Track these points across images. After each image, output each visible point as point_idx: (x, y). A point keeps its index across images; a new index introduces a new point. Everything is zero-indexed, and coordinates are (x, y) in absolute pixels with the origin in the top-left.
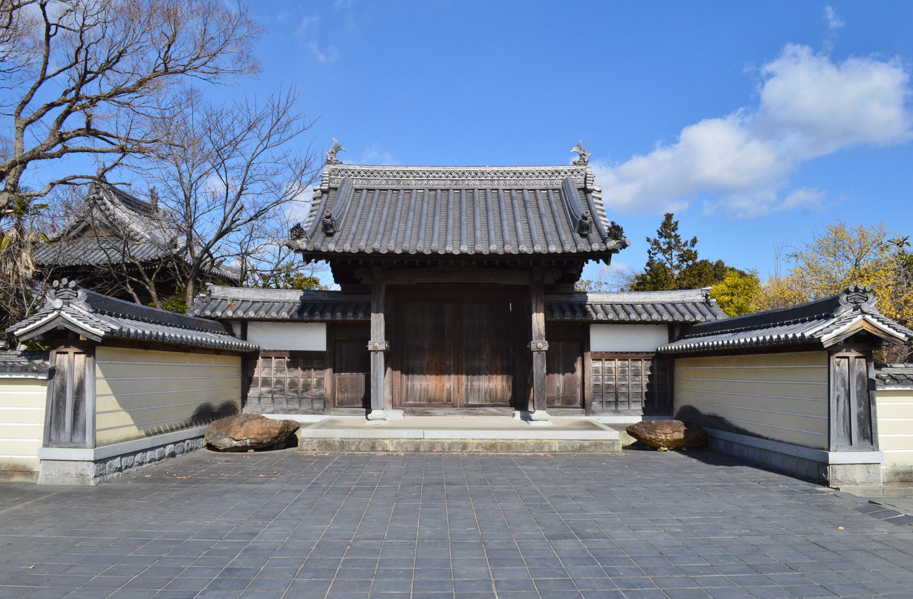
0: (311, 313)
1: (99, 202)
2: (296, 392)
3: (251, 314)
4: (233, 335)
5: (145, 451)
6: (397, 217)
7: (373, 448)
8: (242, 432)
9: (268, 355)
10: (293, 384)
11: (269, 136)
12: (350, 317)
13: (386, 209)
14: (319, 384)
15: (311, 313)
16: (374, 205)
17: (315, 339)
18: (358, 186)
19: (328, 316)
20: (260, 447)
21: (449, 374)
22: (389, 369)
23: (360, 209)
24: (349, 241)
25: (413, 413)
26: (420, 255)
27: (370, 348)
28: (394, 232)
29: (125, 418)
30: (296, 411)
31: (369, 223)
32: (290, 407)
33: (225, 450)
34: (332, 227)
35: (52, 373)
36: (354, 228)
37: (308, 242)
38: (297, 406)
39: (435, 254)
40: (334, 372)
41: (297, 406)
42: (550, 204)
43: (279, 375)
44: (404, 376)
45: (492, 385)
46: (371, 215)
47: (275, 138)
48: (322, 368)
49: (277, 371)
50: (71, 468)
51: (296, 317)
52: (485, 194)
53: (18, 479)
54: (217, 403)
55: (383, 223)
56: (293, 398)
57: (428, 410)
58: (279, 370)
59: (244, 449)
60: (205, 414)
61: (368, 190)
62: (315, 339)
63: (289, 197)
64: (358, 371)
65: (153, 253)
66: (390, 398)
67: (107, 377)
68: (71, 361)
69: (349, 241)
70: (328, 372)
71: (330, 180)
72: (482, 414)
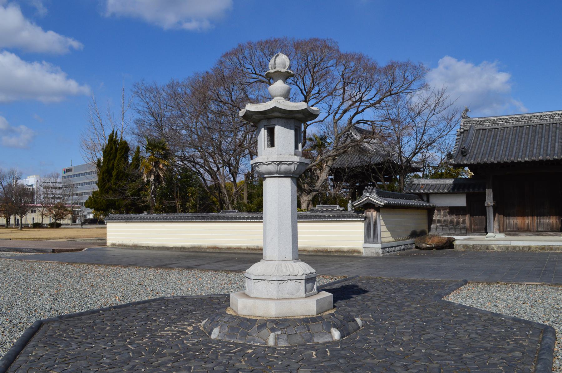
0: (458, 189)
1: (350, 136)
2: (453, 225)
3: (431, 191)
4: (423, 200)
5: (395, 247)
6: (496, 144)
7: (487, 248)
8: (430, 242)
9: (439, 209)
10: (452, 222)
11: (434, 109)
12: (476, 190)
13: (491, 140)
14: (464, 221)
15: (458, 189)
16: (485, 138)
17: (461, 201)
18: (478, 128)
19: (466, 191)
20: (438, 247)
21: (528, 216)
22: (497, 215)
23: (479, 141)
24: (473, 159)
25: (510, 235)
26: (506, 163)
27: (486, 205)
28: (494, 152)
29: (388, 234)
30: (454, 234)
31: (483, 148)
32: (450, 232)
33: (424, 249)
34: (465, 152)
35: (365, 218)
36: (475, 152)
37: (455, 160)
38: (454, 232)
39: (513, 162)
40: (471, 216)
41: (454, 232)
42: (389, 247)
43: (445, 218)
44: (505, 218)
45: (551, 221)
46: (484, 144)
47: (437, 110)
48: (465, 214)
49: (444, 216)
50: (374, 250)
51: (451, 191)
52: (543, 127)
53: (355, 254)
54: (418, 230)
55: (489, 148)
56: (452, 228)
57: (517, 233)
58: (445, 216)
59: (431, 248)
60: (414, 234)
61: (483, 130)
62: (461, 201)
63: (445, 133)
64: (482, 215)
65: (378, 159)
66: (498, 228)
67: (383, 219)
68: (372, 214)
69: (473, 159)
70: (467, 217)
71: (465, 126)
72: (545, 236)
